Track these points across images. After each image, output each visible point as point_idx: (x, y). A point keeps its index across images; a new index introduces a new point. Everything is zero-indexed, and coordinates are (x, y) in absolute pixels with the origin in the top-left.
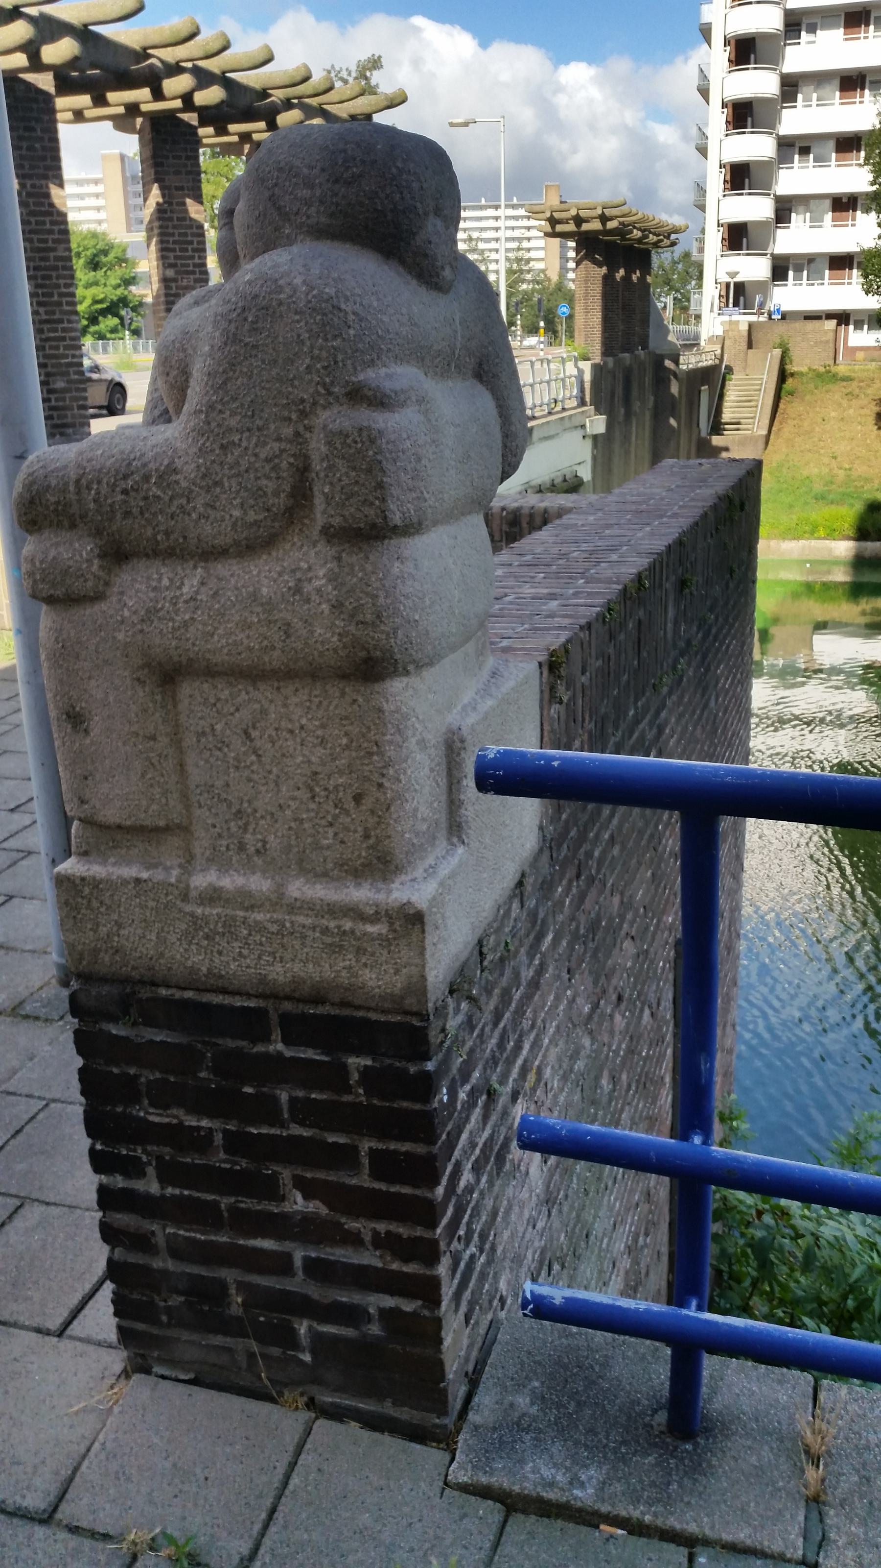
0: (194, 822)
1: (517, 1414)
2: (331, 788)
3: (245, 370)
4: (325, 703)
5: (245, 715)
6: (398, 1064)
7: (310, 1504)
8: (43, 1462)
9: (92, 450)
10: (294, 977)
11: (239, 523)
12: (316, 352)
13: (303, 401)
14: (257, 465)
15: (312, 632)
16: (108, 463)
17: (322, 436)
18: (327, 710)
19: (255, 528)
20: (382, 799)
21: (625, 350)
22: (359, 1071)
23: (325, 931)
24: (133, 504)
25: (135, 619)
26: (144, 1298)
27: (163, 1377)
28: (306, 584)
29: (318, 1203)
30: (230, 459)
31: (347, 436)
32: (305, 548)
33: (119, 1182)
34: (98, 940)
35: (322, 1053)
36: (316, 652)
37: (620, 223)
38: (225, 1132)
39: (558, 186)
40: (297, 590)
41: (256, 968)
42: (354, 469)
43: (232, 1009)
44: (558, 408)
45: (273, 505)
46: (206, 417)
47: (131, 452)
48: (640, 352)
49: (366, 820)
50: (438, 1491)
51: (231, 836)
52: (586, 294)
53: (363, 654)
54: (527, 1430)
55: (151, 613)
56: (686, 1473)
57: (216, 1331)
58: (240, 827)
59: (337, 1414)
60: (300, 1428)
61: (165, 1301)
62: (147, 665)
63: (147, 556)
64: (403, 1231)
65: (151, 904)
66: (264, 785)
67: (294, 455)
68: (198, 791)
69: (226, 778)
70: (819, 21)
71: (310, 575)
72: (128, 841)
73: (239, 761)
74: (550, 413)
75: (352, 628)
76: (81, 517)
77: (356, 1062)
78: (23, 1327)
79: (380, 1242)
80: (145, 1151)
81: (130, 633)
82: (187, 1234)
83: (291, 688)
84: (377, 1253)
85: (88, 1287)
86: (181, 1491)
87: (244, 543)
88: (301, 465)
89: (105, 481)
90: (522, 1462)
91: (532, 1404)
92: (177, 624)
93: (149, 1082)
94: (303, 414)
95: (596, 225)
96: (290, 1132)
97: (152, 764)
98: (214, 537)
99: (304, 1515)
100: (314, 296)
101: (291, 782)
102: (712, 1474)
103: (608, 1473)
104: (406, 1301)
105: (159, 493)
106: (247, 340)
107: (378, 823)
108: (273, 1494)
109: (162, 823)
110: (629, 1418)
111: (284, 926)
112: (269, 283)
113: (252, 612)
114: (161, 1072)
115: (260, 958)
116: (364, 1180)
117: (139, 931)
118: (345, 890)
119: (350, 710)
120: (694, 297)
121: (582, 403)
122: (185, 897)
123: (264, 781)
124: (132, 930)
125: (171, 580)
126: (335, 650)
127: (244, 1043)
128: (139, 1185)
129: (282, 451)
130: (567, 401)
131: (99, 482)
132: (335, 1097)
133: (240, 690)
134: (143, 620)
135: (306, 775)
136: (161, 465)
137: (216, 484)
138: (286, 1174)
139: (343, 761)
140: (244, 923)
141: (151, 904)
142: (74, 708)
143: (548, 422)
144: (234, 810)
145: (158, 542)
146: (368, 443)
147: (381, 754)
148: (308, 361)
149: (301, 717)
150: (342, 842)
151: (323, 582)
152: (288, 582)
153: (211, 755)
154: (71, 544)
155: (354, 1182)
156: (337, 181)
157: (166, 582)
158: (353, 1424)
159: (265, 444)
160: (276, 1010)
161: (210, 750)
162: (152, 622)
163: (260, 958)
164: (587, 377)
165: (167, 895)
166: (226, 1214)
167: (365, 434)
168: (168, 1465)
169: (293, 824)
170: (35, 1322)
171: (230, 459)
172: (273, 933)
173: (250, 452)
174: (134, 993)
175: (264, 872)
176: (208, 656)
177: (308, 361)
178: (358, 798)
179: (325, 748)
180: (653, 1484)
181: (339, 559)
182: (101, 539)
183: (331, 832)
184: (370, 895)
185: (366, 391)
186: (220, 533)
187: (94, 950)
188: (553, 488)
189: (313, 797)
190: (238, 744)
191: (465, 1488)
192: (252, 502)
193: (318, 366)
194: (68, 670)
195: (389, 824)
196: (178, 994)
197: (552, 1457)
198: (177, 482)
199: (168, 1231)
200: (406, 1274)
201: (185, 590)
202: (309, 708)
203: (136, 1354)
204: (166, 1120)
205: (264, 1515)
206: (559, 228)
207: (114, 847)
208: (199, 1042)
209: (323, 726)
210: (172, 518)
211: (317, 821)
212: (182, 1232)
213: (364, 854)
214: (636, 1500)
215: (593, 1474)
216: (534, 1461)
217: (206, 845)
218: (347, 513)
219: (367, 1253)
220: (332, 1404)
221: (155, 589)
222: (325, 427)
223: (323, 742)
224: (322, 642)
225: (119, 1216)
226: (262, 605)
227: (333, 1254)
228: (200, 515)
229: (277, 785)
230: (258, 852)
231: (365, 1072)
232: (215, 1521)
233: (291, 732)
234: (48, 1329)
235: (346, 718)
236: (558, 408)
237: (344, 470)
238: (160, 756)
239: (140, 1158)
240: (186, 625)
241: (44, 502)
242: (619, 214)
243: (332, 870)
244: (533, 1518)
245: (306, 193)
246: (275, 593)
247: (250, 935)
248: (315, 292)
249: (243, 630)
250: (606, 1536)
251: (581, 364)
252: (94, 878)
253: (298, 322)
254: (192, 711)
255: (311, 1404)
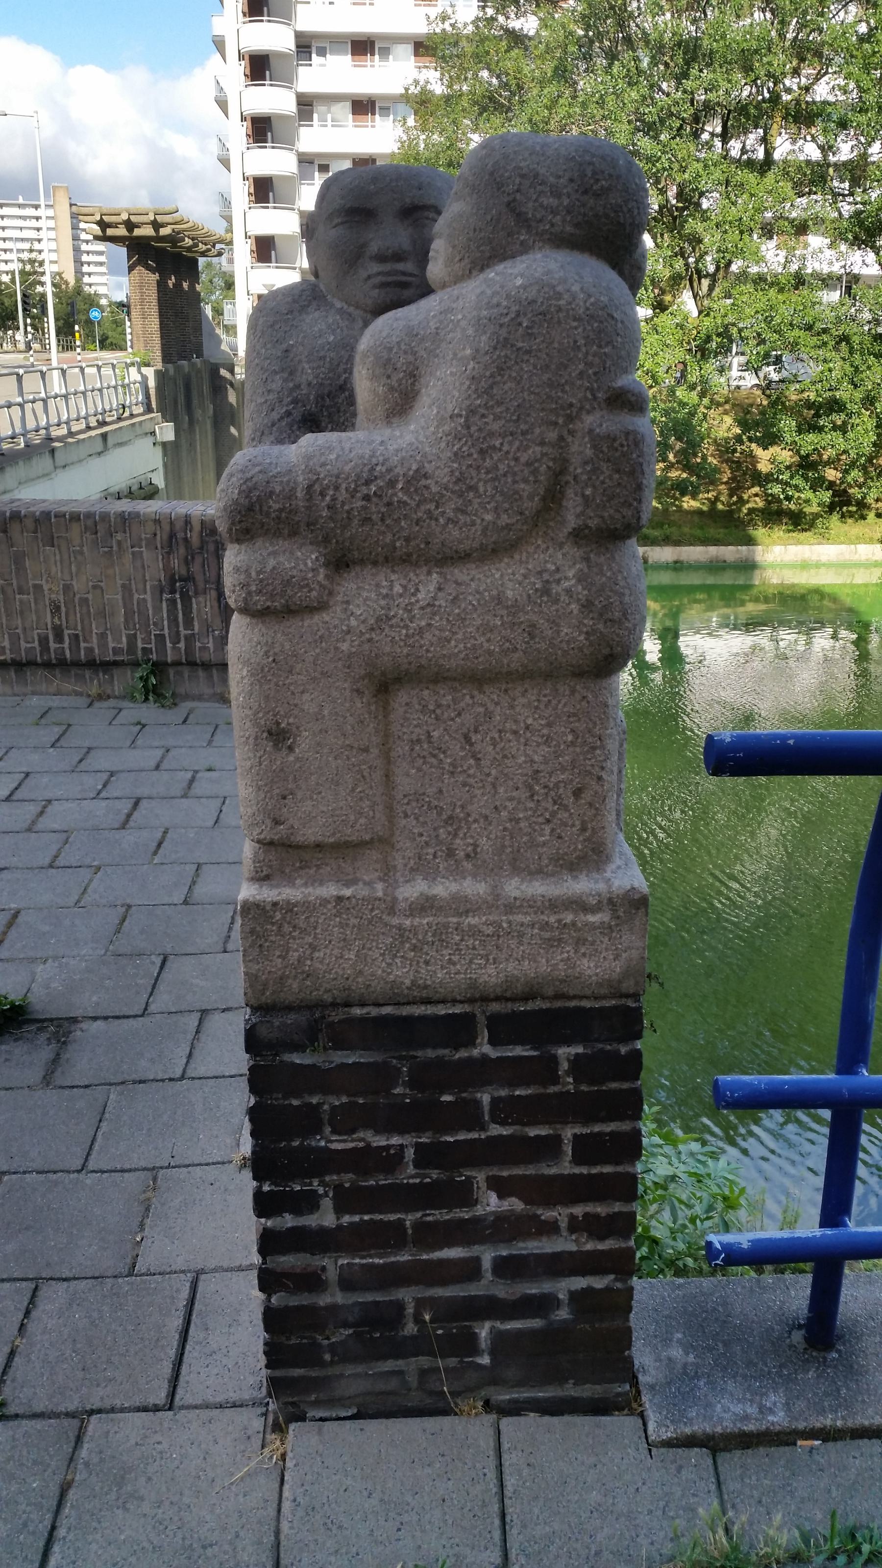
0: (398, 833)
1: (679, 1366)
2: (551, 785)
3: (514, 374)
4: (554, 702)
5: (468, 719)
6: (609, 1047)
7: (536, 1498)
8: (237, 1536)
9: (322, 454)
10: (507, 976)
11: (490, 527)
12: (590, 358)
13: (571, 405)
14: (516, 469)
15: (558, 632)
16: (347, 468)
17: (587, 439)
18: (555, 709)
19: (506, 531)
20: (600, 790)
21: (184, 358)
22: (568, 1060)
23: (546, 926)
24: (374, 509)
25: (362, 628)
26: (305, 1341)
27: (322, 1420)
28: (554, 586)
29: (514, 1200)
30: (488, 463)
31: (615, 440)
32: (551, 551)
33: (288, 1221)
34: (286, 967)
35: (531, 1049)
36: (559, 652)
37: (173, 230)
38: (418, 1146)
39: (67, 188)
40: (545, 591)
41: (465, 973)
42: (618, 471)
43: (436, 1019)
44: (127, 414)
45: (527, 509)
46: (466, 421)
47: (371, 457)
48: (195, 360)
49: (584, 814)
50: (646, 1452)
51: (440, 843)
52: (142, 301)
53: (606, 651)
54: (697, 1376)
55: (382, 621)
56: (845, 1377)
57: (385, 1357)
58: (449, 833)
59: (514, 1409)
60: (491, 1432)
61: (328, 1338)
62: (369, 675)
63: (375, 563)
64: (600, 1209)
65: (353, 921)
66: (479, 788)
67: (554, 460)
68: (406, 801)
69: (440, 784)
70: (328, 45)
71: (557, 576)
72: (319, 859)
73: (455, 767)
74: (120, 419)
75: (601, 626)
76: (308, 525)
77: (565, 1052)
78: (122, 1410)
79: (575, 1226)
80: (322, 1183)
81: (356, 643)
82: (364, 1261)
83: (520, 689)
84: (574, 1237)
85: (172, 1353)
86: (402, 1524)
87: (490, 547)
88: (558, 469)
89: (344, 486)
90: (709, 1405)
91: (687, 1354)
92: (411, 631)
93: (333, 1108)
94: (570, 419)
95: (148, 231)
96: (489, 1134)
97: (363, 777)
98: (460, 542)
99: (536, 1511)
100: (592, 304)
101: (511, 783)
102: (866, 1372)
103: (785, 1395)
104: (597, 1278)
105: (405, 498)
106: (520, 345)
107: (595, 816)
108: (495, 1500)
109: (367, 837)
110: (773, 1343)
111: (500, 926)
112: (546, 289)
113: (495, 616)
114: (348, 1096)
115: (471, 962)
116: (566, 1167)
117: (336, 952)
118: (565, 884)
119: (578, 707)
120: (227, 308)
121: (149, 410)
122: (392, 910)
123: (480, 785)
124: (328, 951)
125: (405, 587)
126: (581, 649)
127: (446, 1052)
128: (311, 1221)
129: (544, 455)
130: (134, 407)
131: (337, 488)
132: (542, 1091)
133: (465, 695)
134: (372, 629)
135: (526, 775)
136: (410, 469)
137: (471, 488)
138: (480, 1177)
139: (567, 758)
140: (456, 929)
141: (353, 921)
142: (278, 724)
143: (120, 428)
144: (444, 817)
145: (395, 548)
146: (633, 447)
147: (603, 747)
148: (581, 366)
149: (528, 717)
150: (560, 837)
151: (573, 582)
152: (535, 584)
153: (424, 763)
154: (292, 553)
155: (553, 1171)
156: (586, 192)
157: (397, 589)
158: (532, 1414)
159: (527, 448)
160: (484, 1012)
161: (424, 757)
162: (383, 630)
163: (471, 962)
164: (152, 383)
165: (372, 910)
166: (410, 1231)
167: (631, 437)
168: (374, 1501)
169: (508, 825)
170: (137, 1401)
171: (488, 463)
172: (488, 935)
173: (510, 456)
174: (323, 1017)
175: (474, 876)
176: (441, 662)
177: (581, 366)
178: (577, 793)
179: (550, 747)
180: (826, 1394)
181: (587, 559)
182: (326, 547)
183: (547, 829)
184: (592, 885)
185: (629, 395)
186: (468, 538)
187: (281, 979)
188: (131, 494)
189: (532, 796)
190: (456, 749)
191: (669, 1444)
192: (506, 505)
193: (590, 372)
194: (277, 685)
195: (604, 815)
196: (374, 1012)
197: (732, 1395)
198: (427, 487)
199: (340, 1262)
200: (602, 1252)
201: (420, 596)
202: (537, 708)
203: (286, 1404)
204: (351, 1145)
205: (497, 1522)
206: (110, 232)
207: (301, 868)
208: (394, 1058)
209: (549, 725)
210: (417, 524)
211: (534, 819)
212: (357, 1261)
213: (580, 847)
214: (823, 1412)
215: (773, 1399)
216: (719, 1402)
217: (411, 855)
218: (606, 514)
219: (562, 1239)
220: (509, 1401)
221: (386, 596)
222: (591, 431)
223: (548, 740)
224: (568, 642)
225: (283, 1259)
226: (507, 607)
227: (526, 1249)
228: (449, 519)
229: (494, 786)
230: (468, 856)
231: (576, 1062)
232: (452, 1541)
233: (515, 732)
234: (155, 1405)
235: (575, 715)
236: (127, 414)
237: (607, 473)
238: (370, 767)
239: (316, 1191)
240: (421, 631)
241: (265, 508)
242: (171, 221)
243: (547, 866)
244: (738, 1453)
245: (553, 202)
246: (521, 595)
247: (462, 940)
248: (592, 300)
249: (484, 634)
250: (808, 1449)
251: (144, 370)
252: (288, 902)
253: (576, 328)
254: (408, 719)
255: (488, 1406)
